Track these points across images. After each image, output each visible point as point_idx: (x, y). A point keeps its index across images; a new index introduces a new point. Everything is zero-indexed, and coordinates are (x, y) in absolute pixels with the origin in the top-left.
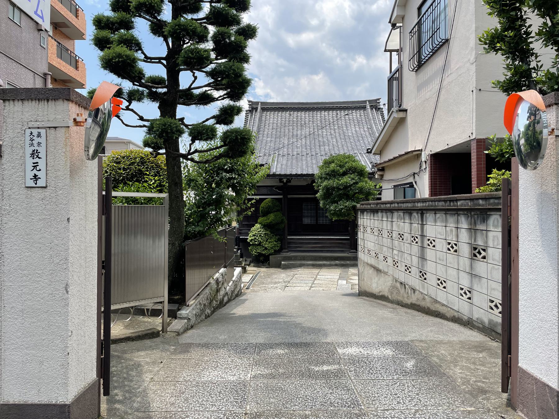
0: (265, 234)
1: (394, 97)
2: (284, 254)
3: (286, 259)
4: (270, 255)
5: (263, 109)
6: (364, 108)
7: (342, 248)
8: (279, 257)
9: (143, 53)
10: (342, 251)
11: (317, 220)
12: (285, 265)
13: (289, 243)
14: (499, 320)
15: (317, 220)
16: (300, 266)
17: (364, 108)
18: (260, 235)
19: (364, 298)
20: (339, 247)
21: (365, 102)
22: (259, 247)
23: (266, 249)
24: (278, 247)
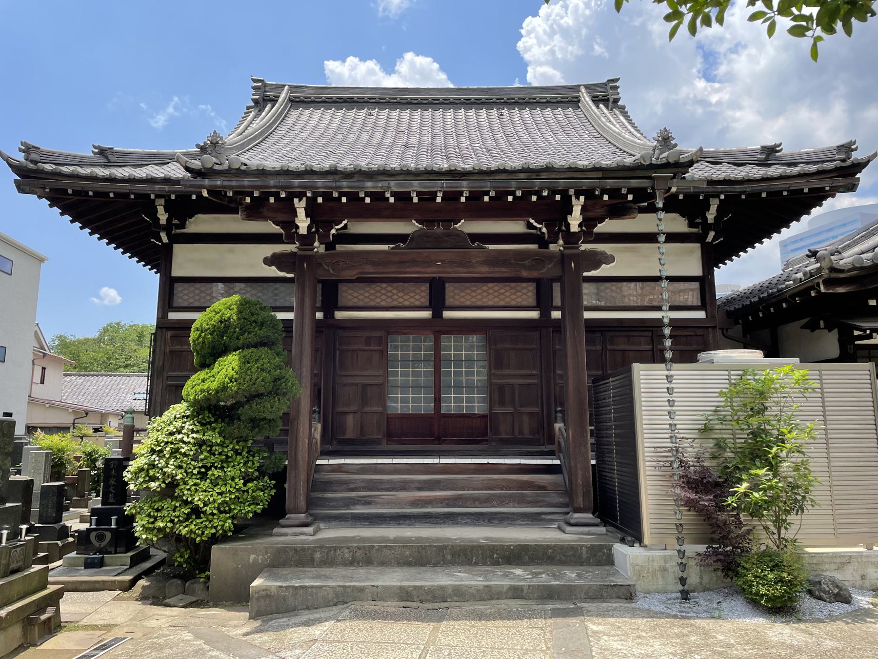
0: (200, 444)
1: (544, 401)
2: (289, 535)
3: (281, 561)
4: (215, 539)
5: (295, 102)
6: (575, 103)
7: (535, 503)
8: (252, 550)
9: (434, 432)
10: (535, 519)
11: (438, 400)
12: (266, 595)
13: (328, 486)
14: (347, 437)
15: (438, 400)
16: (342, 601)
17: (575, 103)
18: (175, 452)
19: (519, 522)
20: (521, 501)
21: (577, 87)
22: (166, 504)
23: (196, 512)
24: (255, 501)
